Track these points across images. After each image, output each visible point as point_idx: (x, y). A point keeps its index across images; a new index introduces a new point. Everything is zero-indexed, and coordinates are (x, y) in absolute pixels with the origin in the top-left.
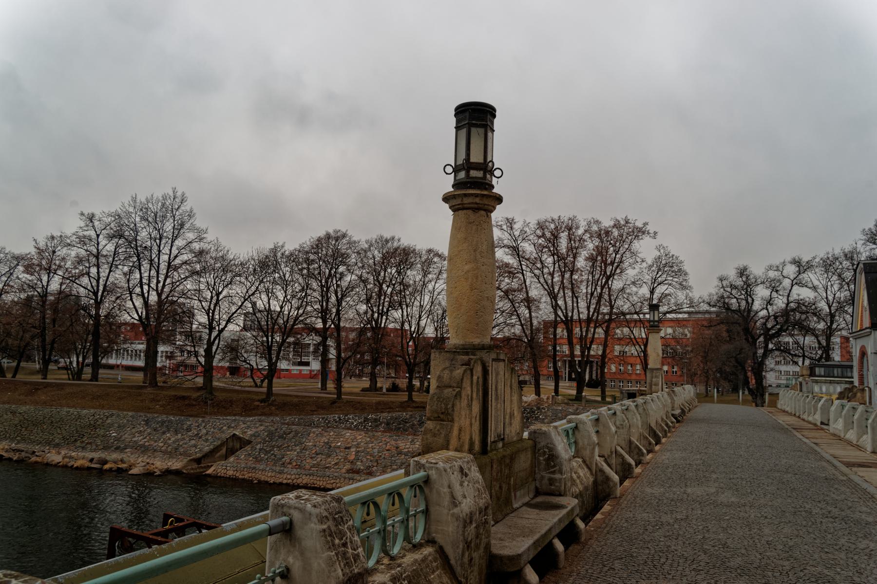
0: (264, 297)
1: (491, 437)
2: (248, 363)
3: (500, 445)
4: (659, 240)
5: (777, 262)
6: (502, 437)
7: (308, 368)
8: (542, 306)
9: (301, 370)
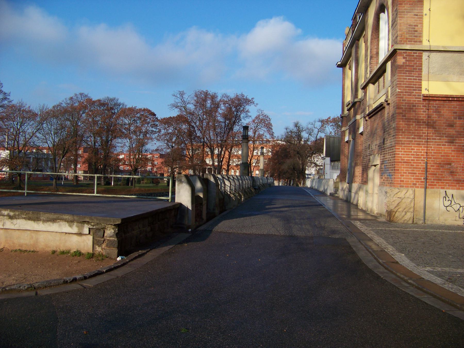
4: (258, 107)
5: (312, 121)
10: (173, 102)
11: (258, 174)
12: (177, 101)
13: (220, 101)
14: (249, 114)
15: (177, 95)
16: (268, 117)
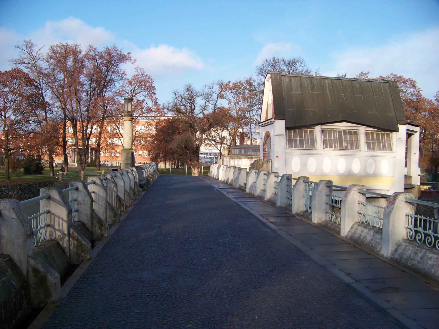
4: (137, 64)
10: (17, 57)
11: (141, 154)
12: (23, 56)
13: (85, 56)
16: (149, 77)
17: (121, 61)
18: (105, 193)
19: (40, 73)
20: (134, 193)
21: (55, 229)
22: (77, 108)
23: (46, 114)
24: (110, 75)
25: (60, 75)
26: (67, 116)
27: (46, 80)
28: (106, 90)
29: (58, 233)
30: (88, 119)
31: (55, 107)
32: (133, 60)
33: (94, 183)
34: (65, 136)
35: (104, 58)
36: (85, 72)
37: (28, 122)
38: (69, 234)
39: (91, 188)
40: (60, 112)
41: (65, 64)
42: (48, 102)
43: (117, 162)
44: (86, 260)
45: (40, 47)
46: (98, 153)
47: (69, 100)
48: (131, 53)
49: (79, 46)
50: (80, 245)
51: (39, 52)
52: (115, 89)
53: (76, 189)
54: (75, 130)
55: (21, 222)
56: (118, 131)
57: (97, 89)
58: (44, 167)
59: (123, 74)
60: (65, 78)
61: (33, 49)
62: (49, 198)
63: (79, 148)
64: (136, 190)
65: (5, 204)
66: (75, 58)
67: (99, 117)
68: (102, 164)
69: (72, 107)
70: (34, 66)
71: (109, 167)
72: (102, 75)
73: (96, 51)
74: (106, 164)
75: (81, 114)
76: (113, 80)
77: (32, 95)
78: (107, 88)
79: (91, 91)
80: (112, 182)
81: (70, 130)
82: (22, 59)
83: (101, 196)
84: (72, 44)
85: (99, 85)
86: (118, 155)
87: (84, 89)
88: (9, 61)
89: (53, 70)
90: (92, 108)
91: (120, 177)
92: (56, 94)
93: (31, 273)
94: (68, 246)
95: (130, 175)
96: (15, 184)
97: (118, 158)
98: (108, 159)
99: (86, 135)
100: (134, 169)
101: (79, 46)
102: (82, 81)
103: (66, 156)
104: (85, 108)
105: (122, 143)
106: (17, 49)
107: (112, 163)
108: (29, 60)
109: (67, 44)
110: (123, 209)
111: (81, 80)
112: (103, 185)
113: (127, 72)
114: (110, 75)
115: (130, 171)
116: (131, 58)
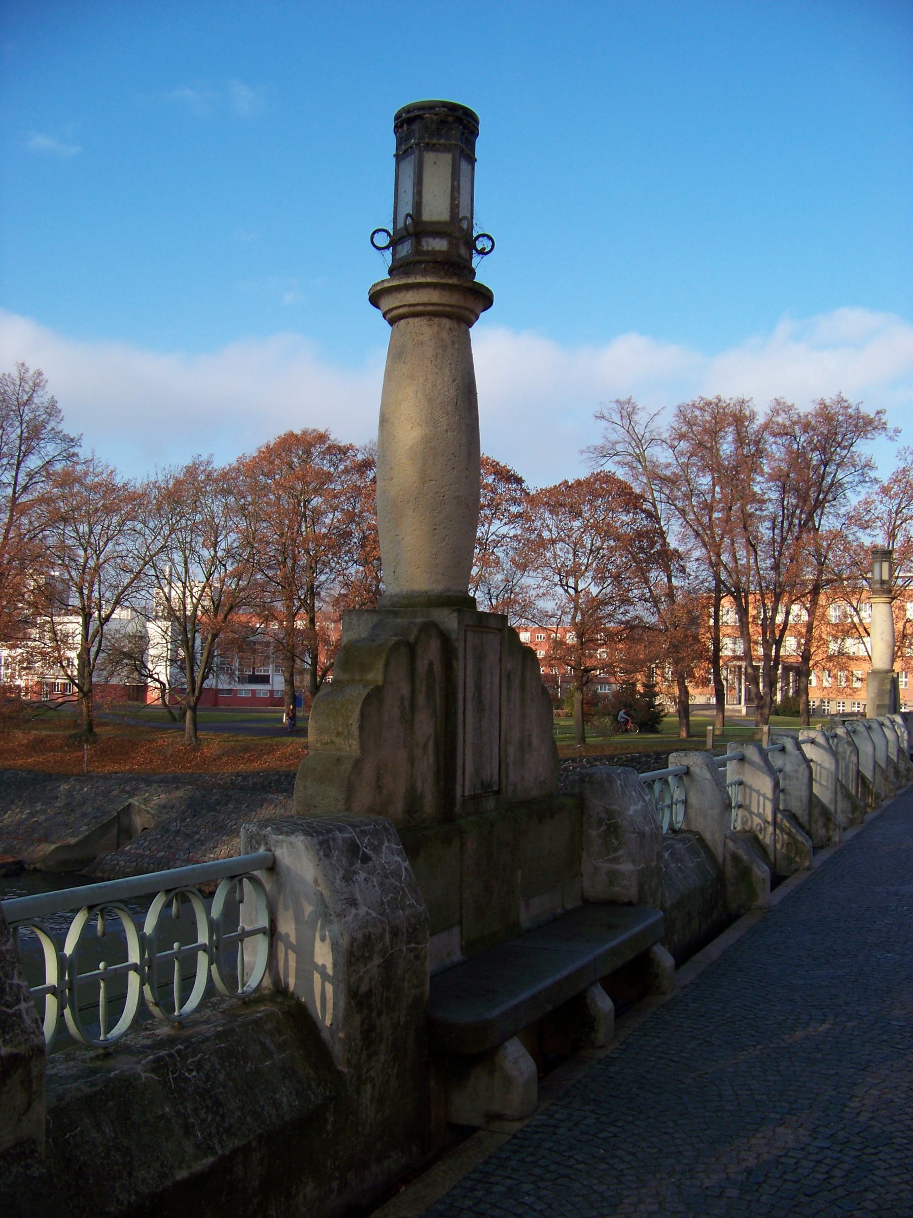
0: (177, 557)
1: (464, 786)
2: (155, 680)
3: (490, 804)
4: (902, 441)
6: (495, 788)
7: (267, 687)
8: (691, 567)
9: (253, 692)
10: (599, 442)
12: (614, 437)
13: (766, 427)
14: (872, 474)
15: (610, 414)
17: (859, 435)
18: (833, 762)
19: (655, 476)
20: (897, 773)
21: (751, 813)
22: (748, 561)
23: (669, 580)
24: (831, 473)
25: (702, 478)
26: (723, 582)
27: (667, 492)
28: (822, 513)
29: (757, 820)
30: (778, 590)
31: (692, 559)
32: (892, 431)
33: (813, 742)
34: (719, 635)
35: (814, 429)
36: (766, 469)
37: (626, 601)
38: (775, 823)
39: (808, 750)
40: (705, 573)
41: (714, 451)
42: (677, 551)
43: (854, 704)
44: (803, 870)
45: (652, 414)
46: (803, 679)
47: (727, 541)
48: (885, 411)
49: (750, 404)
50: (792, 843)
51: (652, 426)
52: (846, 508)
53: (781, 750)
54: (744, 620)
55: (717, 784)
56: (856, 620)
57: (798, 512)
58: (663, 714)
59: (865, 466)
60: (714, 485)
61: (635, 418)
62: (742, 759)
63: (754, 664)
64: (902, 766)
65: (695, 759)
66: (738, 433)
67: (804, 584)
68: (813, 709)
69: (736, 560)
70: (640, 461)
71: (835, 715)
72: (811, 473)
73: (793, 412)
74: (824, 709)
75: (760, 578)
76: (841, 485)
77: (640, 535)
78: (824, 507)
79: (783, 518)
80: (848, 743)
81: (729, 616)
82: (610, 446)
83: (824, 768)
84: (731, 399)
85: (803, 498)
86: (857, 685)
87: (765, 513)
88: (582, 452)
89: (685, 466)
90: (787, 561)
91: (865, 734)
92: (695, 527)
93: (729, 861)
94: (773, 842)
95: (887, 731)
96: (598, 754)
97: (858, 693)
98: (831, 695)
99: (773, 632)
100: (898, 719)
101: (750, 404)
102: (759, 492)
103: (720, 687)
104: (768, 561)
105: (867, 651)
106: (598, 421)
107: (841, 704)
108: (627, 445)
109: (717, 398)
110: (870, 800)
111: (757, 489)
112: (831, 748)
113: (877, 461)
114: (831, 473)
115: (887, 722)
116: (885, 424)
